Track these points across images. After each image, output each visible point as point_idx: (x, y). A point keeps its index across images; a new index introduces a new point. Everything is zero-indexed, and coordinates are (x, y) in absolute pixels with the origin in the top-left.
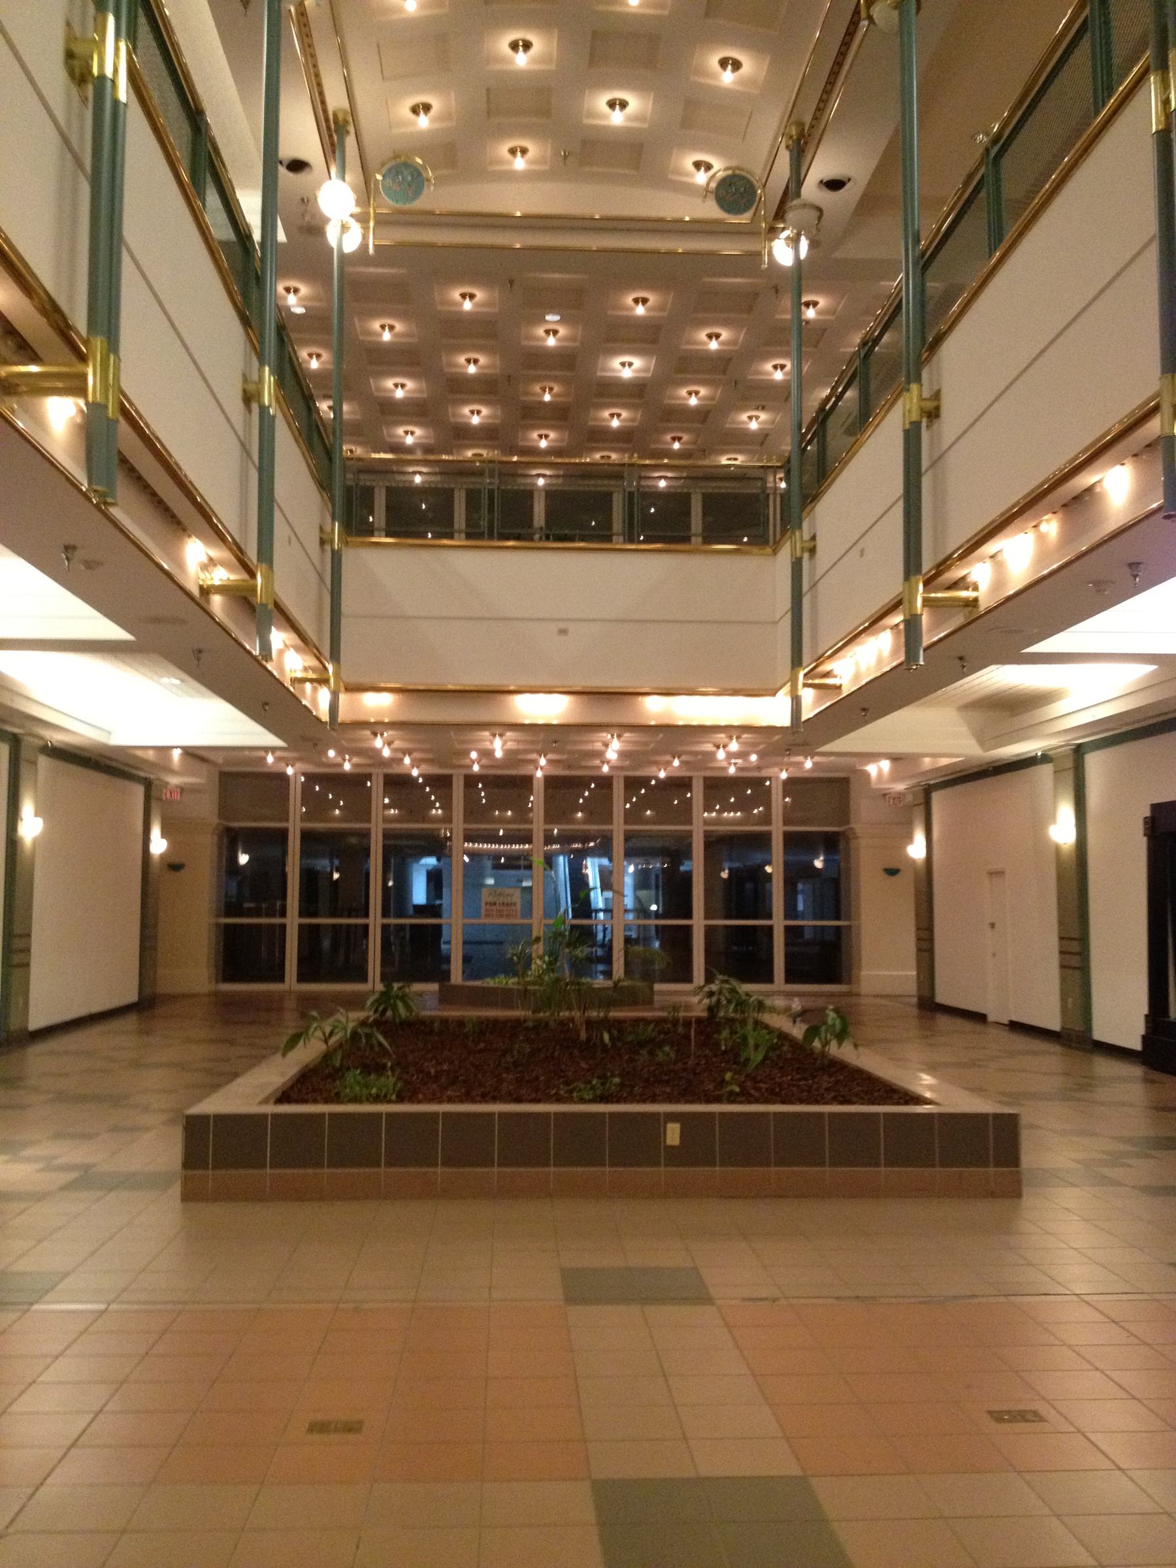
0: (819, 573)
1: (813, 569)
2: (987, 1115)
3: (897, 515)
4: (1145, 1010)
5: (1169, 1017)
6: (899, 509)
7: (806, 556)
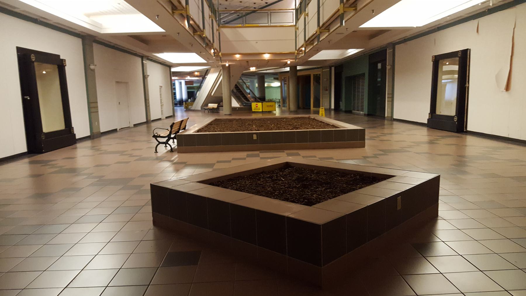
0: (309, 20)
1: (308, 19)
2: (310, 107)
3: (316, 15)
4: (429, 112)
5: (436, 113)
6: (317, 13)
7: (307, 17)
